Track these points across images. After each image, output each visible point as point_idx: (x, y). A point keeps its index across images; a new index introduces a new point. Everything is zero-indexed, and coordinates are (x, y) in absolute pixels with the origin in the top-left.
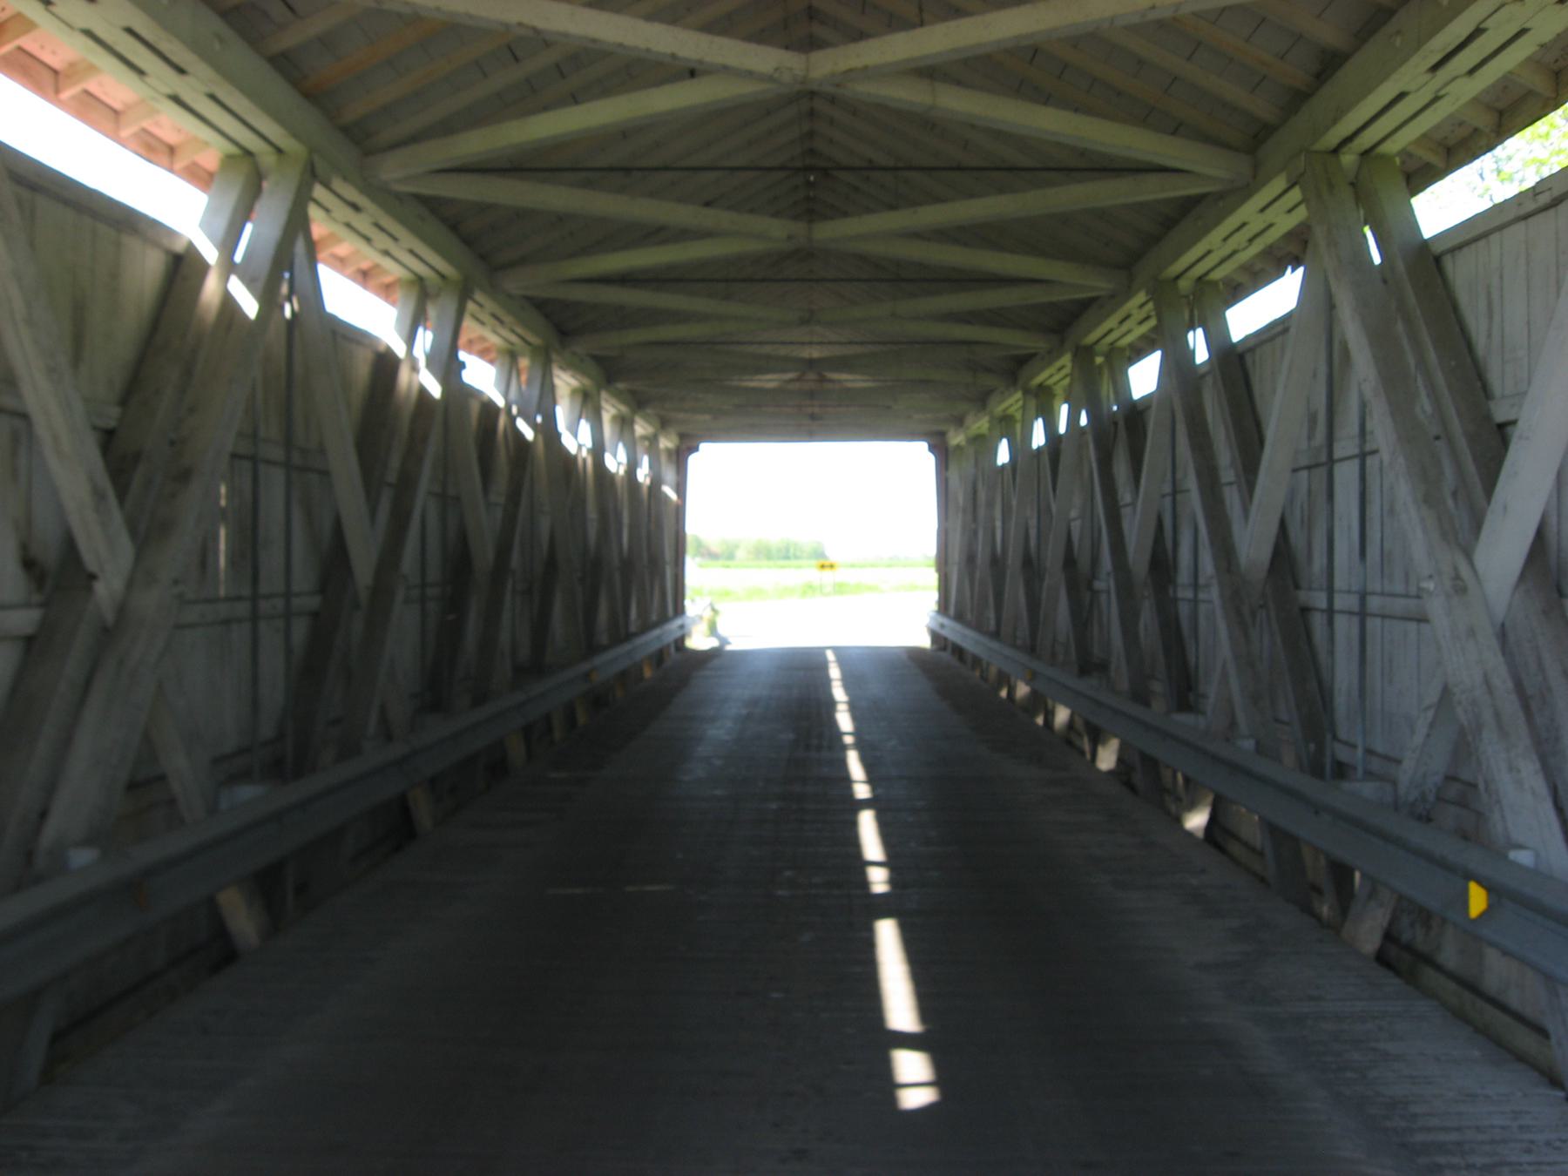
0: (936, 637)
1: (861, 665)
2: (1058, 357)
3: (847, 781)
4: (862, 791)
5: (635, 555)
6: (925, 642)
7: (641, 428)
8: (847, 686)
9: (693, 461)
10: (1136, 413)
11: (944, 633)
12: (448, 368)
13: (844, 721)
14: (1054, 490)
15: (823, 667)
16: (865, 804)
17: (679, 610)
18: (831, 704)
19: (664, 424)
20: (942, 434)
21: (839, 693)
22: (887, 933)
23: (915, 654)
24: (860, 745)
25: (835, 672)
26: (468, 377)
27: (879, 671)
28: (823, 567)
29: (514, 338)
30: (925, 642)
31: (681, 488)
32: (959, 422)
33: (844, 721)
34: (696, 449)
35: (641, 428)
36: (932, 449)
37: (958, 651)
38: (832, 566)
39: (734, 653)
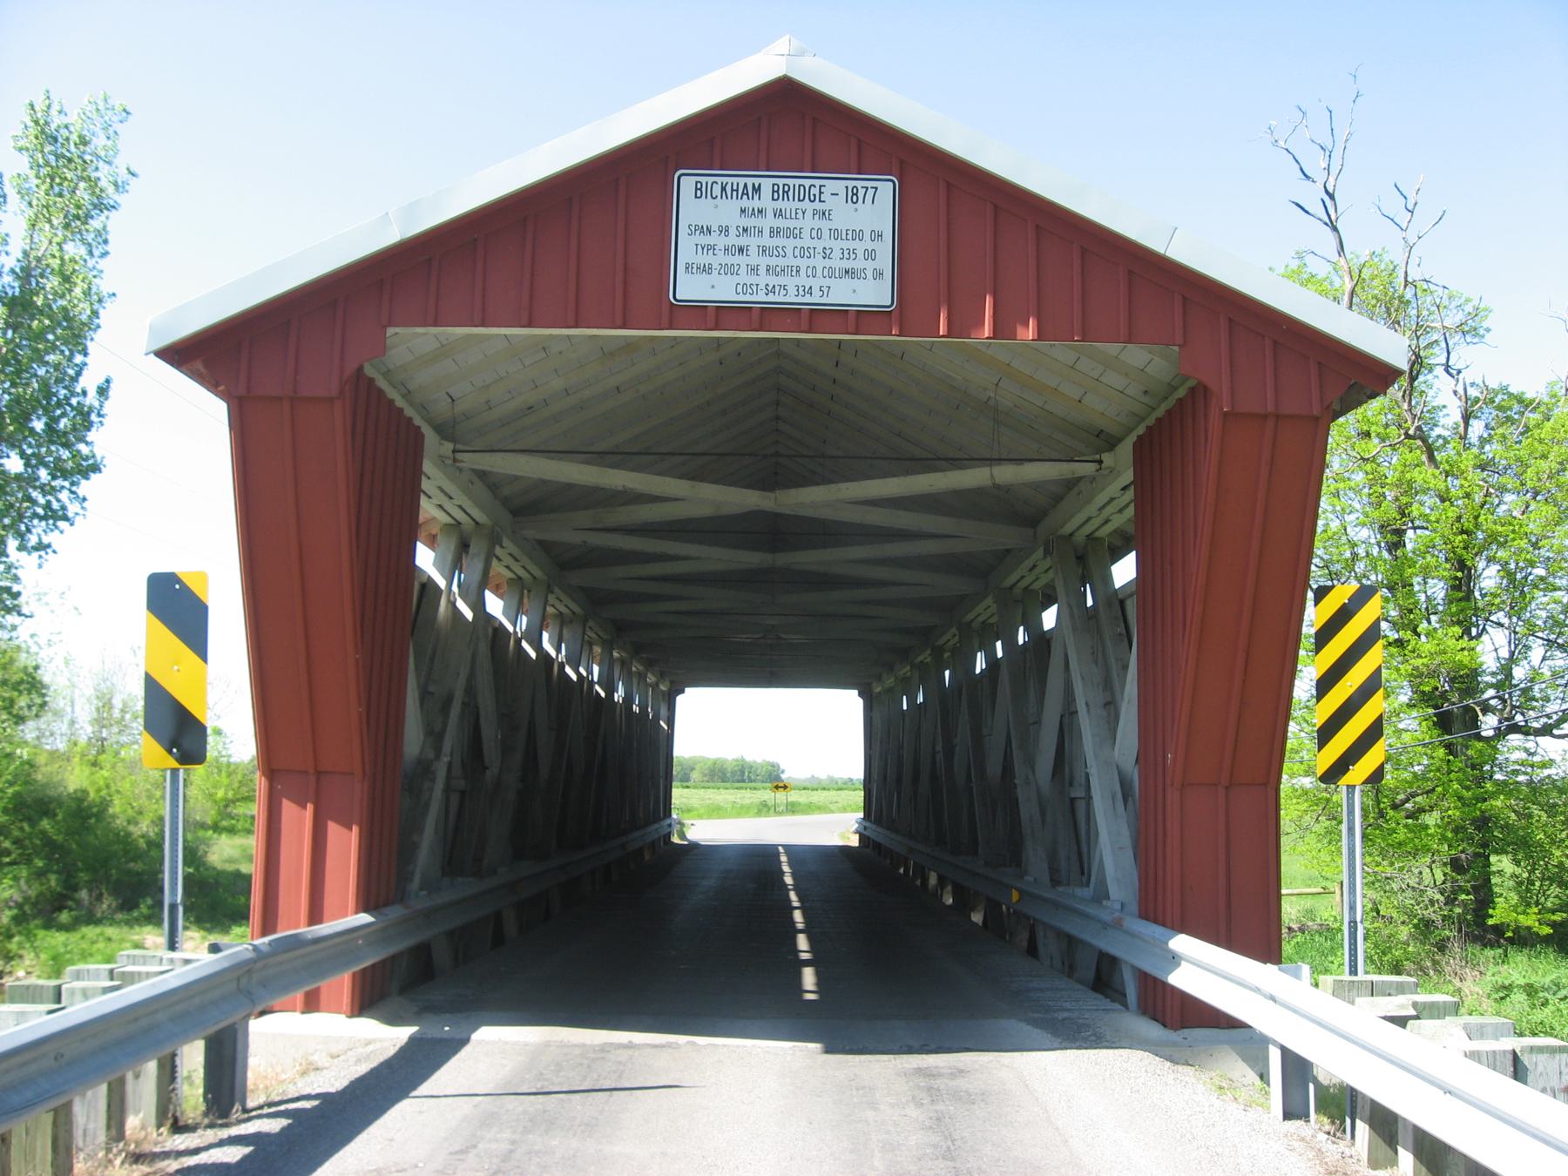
0: (863, 838)
1: (799, 855)
2: (985, 597)
3: (789, 901)
4: (796, 904)
5: (638, 765)
6: (854, 841)
7: (651, 679)
8: (790, 864)
9: (680, 699)
10: (1116, 601)
11: (873, 836)
12: (479, 606)
13: (788, 880)
14: (1066, 656)
15: (778, 854)
16: (807, 963)
17: (668, 813)
18: (783, 873)
19: (662, 676)
20: (870, 684)
21: (786, 868)
22: (800, 926)
23: (845, 850)
24: (797, 888)
25: (784, 858)
26: (490, 609)
27: (819, 864)
28: (777, 787)
29: (521, 572)
30: (854, 841)
31: (671, 722)
32: (879, 678)
33: (788, 880)
34: (683, 692)
35: (651, 679)
36: (860, 695)
37: (877, 846)
38: (785, 787)
39: (694, 847)
